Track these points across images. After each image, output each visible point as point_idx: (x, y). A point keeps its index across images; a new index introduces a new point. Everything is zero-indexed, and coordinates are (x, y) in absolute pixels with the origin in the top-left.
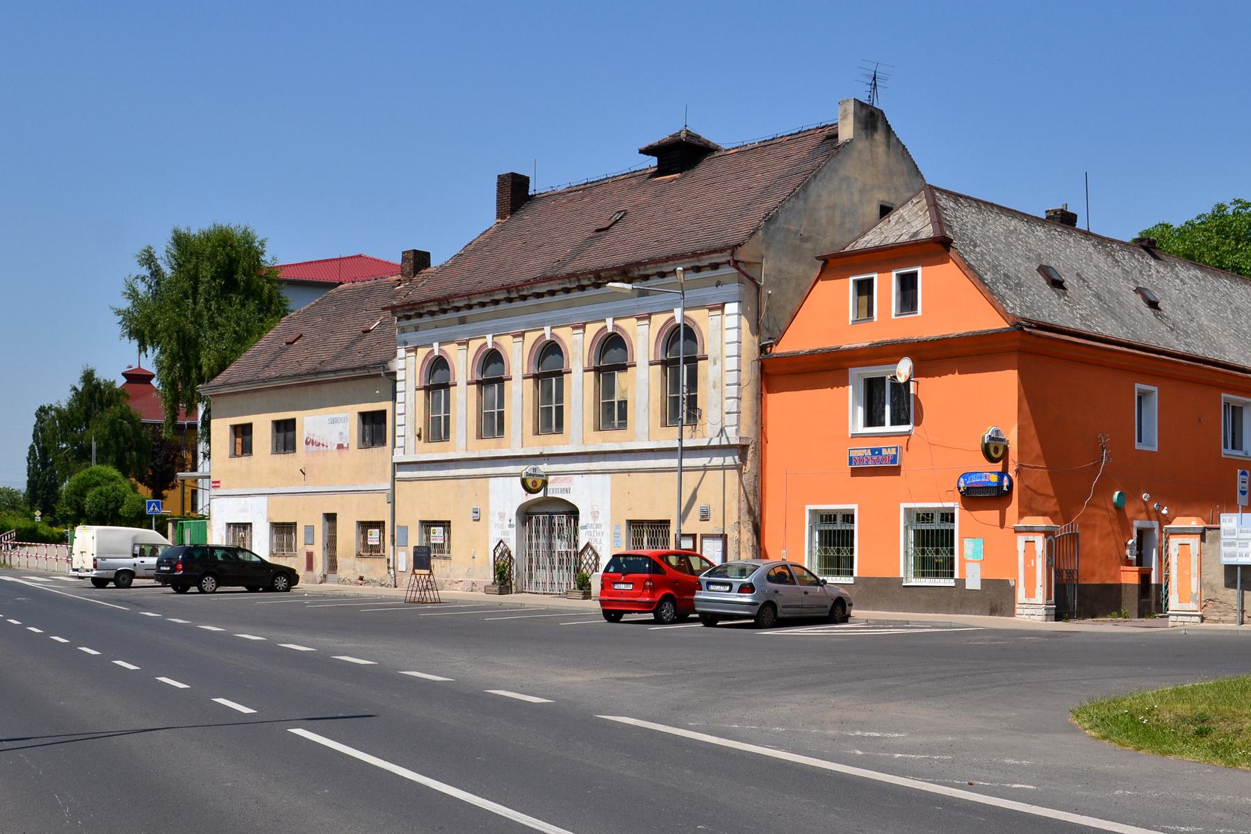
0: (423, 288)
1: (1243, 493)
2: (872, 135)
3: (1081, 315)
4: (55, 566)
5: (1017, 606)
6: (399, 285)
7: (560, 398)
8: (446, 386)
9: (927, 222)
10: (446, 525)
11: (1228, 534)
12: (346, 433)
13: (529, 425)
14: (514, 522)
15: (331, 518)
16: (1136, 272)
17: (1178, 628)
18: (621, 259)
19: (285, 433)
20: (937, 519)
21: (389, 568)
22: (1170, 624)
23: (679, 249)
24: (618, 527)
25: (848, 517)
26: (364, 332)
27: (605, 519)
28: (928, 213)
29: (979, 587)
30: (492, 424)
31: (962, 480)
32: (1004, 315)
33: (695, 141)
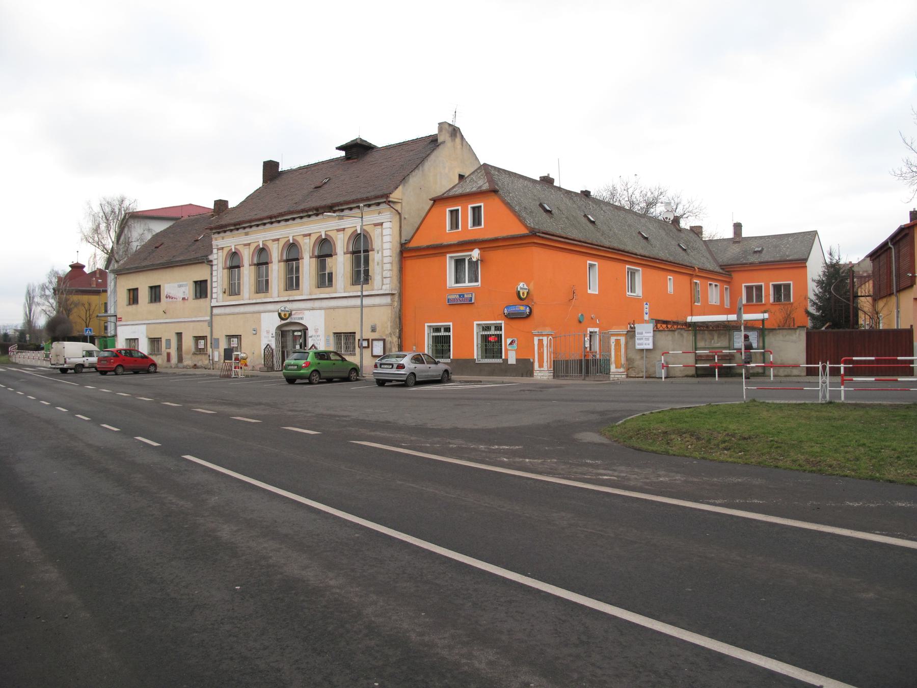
0: (226, 220)
1: (647, 314)
2: (455, 140)
3: (561, 227)
4: (39, 363)
5: (534, 372)
6: (213, 217)
7: (267, 275)
8: (238, 267)
9: (485, 181)
10: (238, 337)
11: (639, 334)
12: (187, 292)
13: (282, 285)
14: (274, 335)
15: (179, 335)
16: (583, 207)
17: (615, 381)
18: (329, 202)
19: (155, 293)
20: (493, 328)
21: (209, 360)
22: (611, 379)
23: (359, 196)
24: (329, 336)
25: (447, 329)
26: (195, 241)
27: (321, 332)
28: (486, 177)
29: (515, 363)
30: (262, 286)
31: (506, 309)
32: (526, 226)
33: (364, 143)
